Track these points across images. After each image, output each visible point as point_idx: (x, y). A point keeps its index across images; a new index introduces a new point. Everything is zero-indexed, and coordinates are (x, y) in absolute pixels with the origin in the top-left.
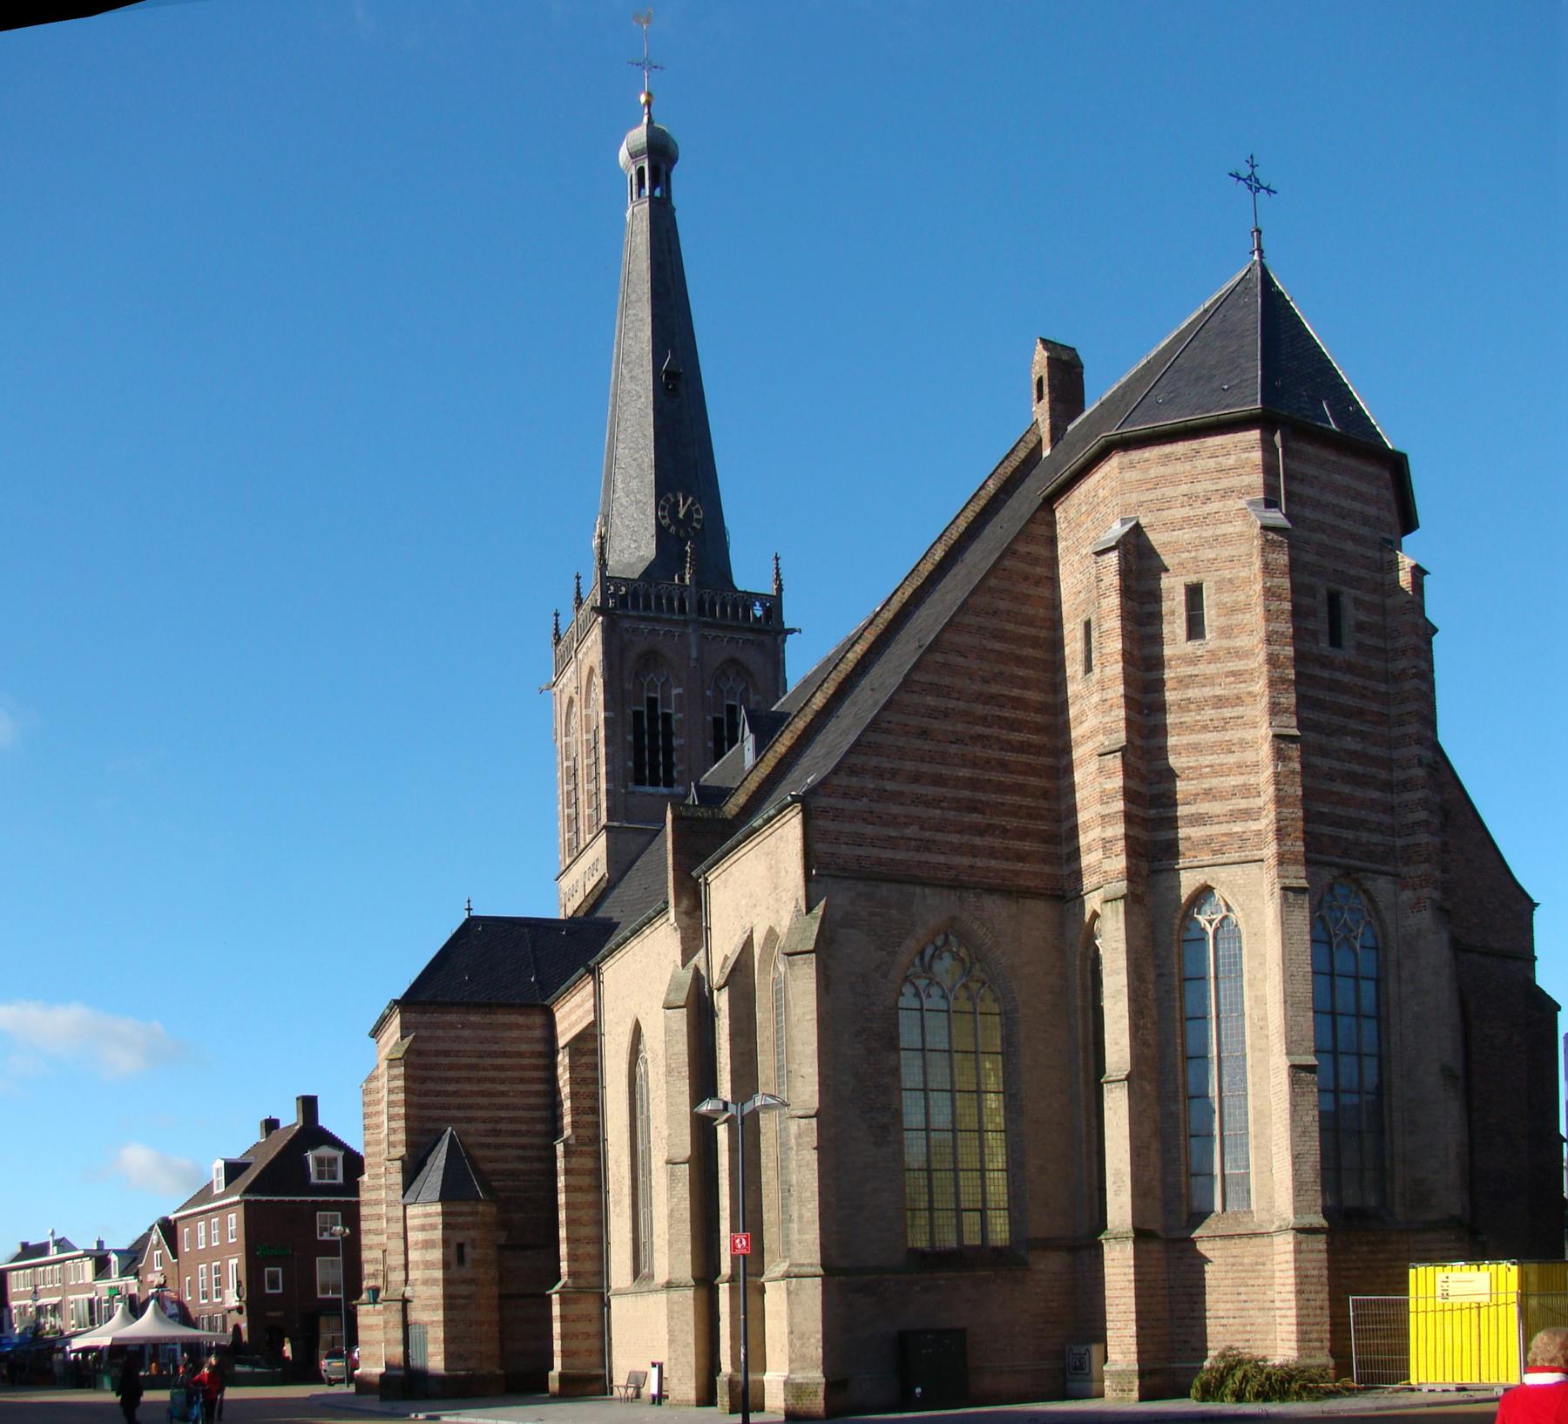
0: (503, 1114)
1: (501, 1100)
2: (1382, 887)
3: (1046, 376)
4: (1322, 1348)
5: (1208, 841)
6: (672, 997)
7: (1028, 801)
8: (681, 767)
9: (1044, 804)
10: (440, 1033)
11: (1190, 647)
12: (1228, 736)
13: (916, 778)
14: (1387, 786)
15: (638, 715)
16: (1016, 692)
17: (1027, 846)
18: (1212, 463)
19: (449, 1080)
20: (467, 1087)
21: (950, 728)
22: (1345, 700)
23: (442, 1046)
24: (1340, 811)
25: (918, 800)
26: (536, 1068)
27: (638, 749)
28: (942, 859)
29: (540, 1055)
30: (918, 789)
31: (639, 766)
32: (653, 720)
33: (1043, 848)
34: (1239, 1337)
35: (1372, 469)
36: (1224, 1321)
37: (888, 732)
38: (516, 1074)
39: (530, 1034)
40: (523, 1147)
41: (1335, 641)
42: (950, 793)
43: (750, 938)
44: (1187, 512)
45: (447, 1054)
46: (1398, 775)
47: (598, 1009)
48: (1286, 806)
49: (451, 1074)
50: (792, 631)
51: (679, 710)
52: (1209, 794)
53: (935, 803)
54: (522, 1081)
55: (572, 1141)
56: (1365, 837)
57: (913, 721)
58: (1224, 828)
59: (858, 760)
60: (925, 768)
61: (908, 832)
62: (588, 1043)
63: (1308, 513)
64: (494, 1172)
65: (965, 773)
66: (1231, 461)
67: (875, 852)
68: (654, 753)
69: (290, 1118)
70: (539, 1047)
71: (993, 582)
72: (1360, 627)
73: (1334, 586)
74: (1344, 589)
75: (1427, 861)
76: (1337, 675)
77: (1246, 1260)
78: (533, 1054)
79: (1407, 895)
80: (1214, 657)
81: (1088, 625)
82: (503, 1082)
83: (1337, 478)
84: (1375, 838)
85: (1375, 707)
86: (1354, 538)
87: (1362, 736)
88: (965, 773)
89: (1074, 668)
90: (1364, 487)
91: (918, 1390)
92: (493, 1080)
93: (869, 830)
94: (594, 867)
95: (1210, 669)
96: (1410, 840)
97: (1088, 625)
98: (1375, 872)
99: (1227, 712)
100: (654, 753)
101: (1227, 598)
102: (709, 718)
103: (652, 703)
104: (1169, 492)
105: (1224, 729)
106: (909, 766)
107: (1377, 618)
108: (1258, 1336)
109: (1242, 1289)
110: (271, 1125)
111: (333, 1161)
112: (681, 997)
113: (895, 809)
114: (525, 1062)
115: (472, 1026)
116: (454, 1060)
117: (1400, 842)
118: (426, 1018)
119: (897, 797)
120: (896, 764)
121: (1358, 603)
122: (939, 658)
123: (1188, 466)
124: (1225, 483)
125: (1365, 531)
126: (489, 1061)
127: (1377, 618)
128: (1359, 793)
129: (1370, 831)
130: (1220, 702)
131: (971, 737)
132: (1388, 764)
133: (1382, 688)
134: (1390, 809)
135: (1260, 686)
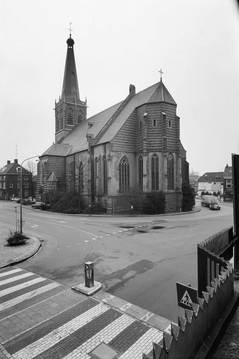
5: (155, 149)
9: (135, 142)
11: (154, 127)
13: (122, 140)
19: (52, 165)
23: (52, 161)
25: (122, 142)
26: (63, 164)
29: (64, 162)
37: (118, 134)
40: (61, 174)
41: (170, 126)
50: (88, 107)
53: (123, 142)
56: (172, 148)
57: (121, 133)
58: (157, 148)
60: (123, 138)
64: (58, 177)
65: (127, 139)
69: (12, 162)
71: (130, 117)
72: (172, 125)
80: (157, 128)
87: (172, 137)
88: (127, 139)
92: (58, 166)
94: (62, 134)
101: (158, 122)
104: (152, 109)
106: (121, 138)
110: (9, 162)
111: (20, 169)
113: (119, 143)
115: (55, 158)
118: (49, 157)
124: (159, 109)
125: (173, 114)
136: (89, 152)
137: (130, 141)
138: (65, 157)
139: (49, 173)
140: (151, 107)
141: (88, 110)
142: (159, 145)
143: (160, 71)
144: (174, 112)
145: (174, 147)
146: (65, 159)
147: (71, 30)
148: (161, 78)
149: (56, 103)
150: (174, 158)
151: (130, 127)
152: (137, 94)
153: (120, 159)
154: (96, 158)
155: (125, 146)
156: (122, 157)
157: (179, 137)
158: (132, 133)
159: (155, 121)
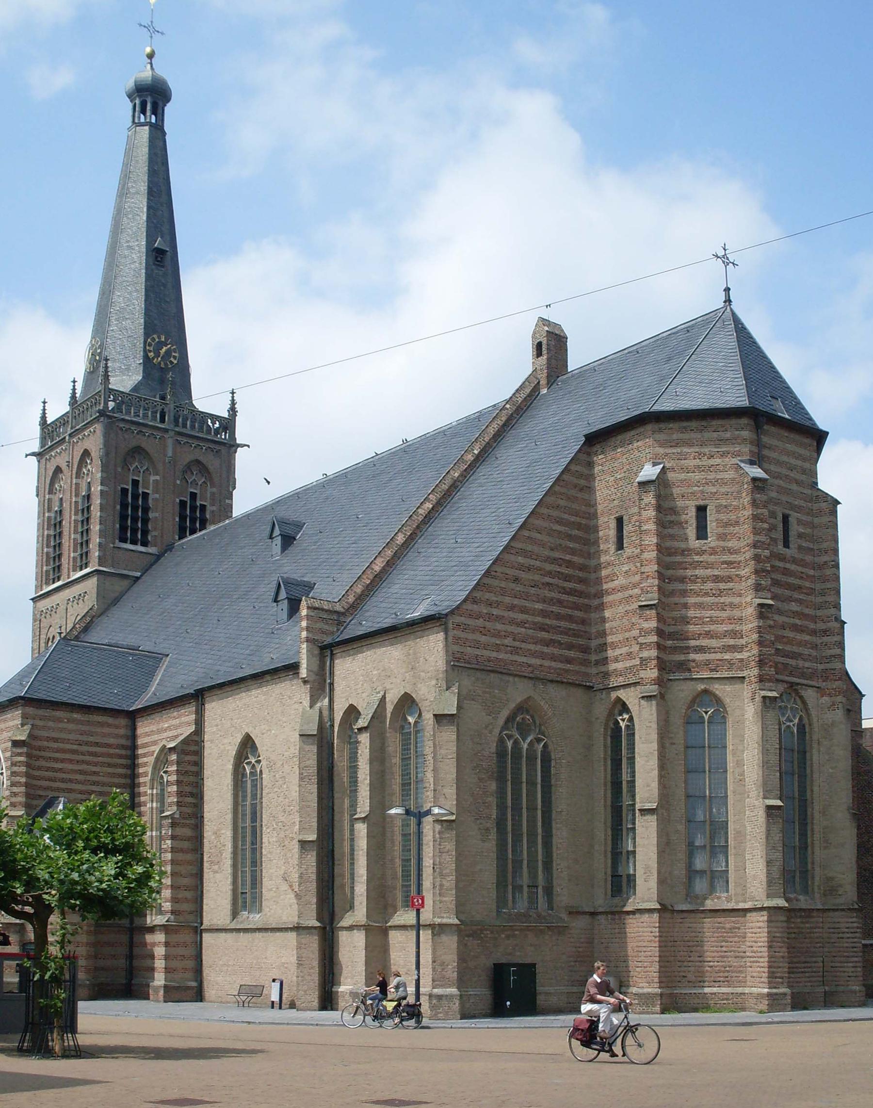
0: (94, 788)
1: (94, 778)
2: (809, 695)
3: (544, 342)
4: (782, 983)
5: (707, 663)
6: (305, 727)
7: (574, 626)
8: (154, 533)
10: (51, 724)
12: (722, 600)
13: (512, 608)
14: (814, 633)
15: (124, 491)
16: (568, 557)
17: (572, 654)
18: (715, 435)
19: (56, 760)
20: (71, 767)
21: (531, 578)
22: (791, 580)
24: (788, 648)
25: (512, 622)
26: (120, 757)
27: (123, 517)
28: (524, 659)
29: (123, 747)
30: (511, 614)
31: (123, 529)
32: (135, 497)
33: (580, 655)
34: (721, 974)
35: (807, 441)
36: (711, 964)
37: (494, 577)
38: (106, 760)
39: (117, 731)
41: (786, 544)
42: (530, 618)
43: (384, 697)
44: (697, 462)
45: (56, 740)
46: (821, 626)
47: (199, 723)
48: (765, 646)
49: (57, 755)
51: (156, 491)
52: (709, 635)
54: (109, 765)
55: (177, 816)
56: (801, 663)
58: (719, 656)
59: (478, 595)
60: (516, 602)
61: (507, 641)
62: (191, 751)
63: (773, 468)
65: (539, 606)
66: (728, 435)
67: (487, 653)
68: (135, 520)
70: (123, 742)
72: (800, 536)
73: (787, 512)
74: (791, 512)
75: (840, 679)
76: (788, 566)
77: (727, 926)
78: (118, 747)
79: (826, 699)
81: (620, 521)
82: (96, 764)
83: (789, 447)
84: (807, 664)
85: (807, 584)
86: (797, 482)
87: (800, 602)
88: (539, 606)
89: (608, 545)
90: (802, 451)
91: (508, 1003)
92: (88, 763)
93: (483, 639)
94: (81, 597)
95: (712, 559)
96: (829, 666)
97: (620, 521)
98: (806, 685)
99: (722, 586)
100: (135, 520)
101: (722, 516)
102: (178, 500)
103: (193, 496)
105: (719, 595)
106: (507, 600)
107: (808, 531)
108: (734, 974)
109: (723, 944)
112: (313, 729)
113: (499, 626)
114: (112, 751)
116: (61, 745)
117: (821, 667)
119: (499, 618)
120: (500, 598)
121: (799, 522)
122: (526, 533)
123: (699, 435)
126: (85, 748)
127: (808, 531)
128: (799, 637)
129: (804, 660)
130: (717, 579)
131: (543, 584)
132: (814, 619)
133: (811, 572)
134: (815, 647)
135: (746, 571)
136: (305, 682)
137: (558, 617)
138: (133, 716)
139: (35, 802)
140: (681, 436)
141: (244, 463)
142: (732, 642)
143: (721, 253)
144: (804, 471)
145: (809, 658)
146: (134, 729)
147: (151, 29)
148: (727, 290)
149: (44, 417)
150: (809, 715)
151: (559, 541)
152: (586, 372)
153: (505, 714)
154: (352, 712)
155: (532, 647)
156: (512, 705)
157: (837, 606)
158: (567, 578)
159: (701, 510)
